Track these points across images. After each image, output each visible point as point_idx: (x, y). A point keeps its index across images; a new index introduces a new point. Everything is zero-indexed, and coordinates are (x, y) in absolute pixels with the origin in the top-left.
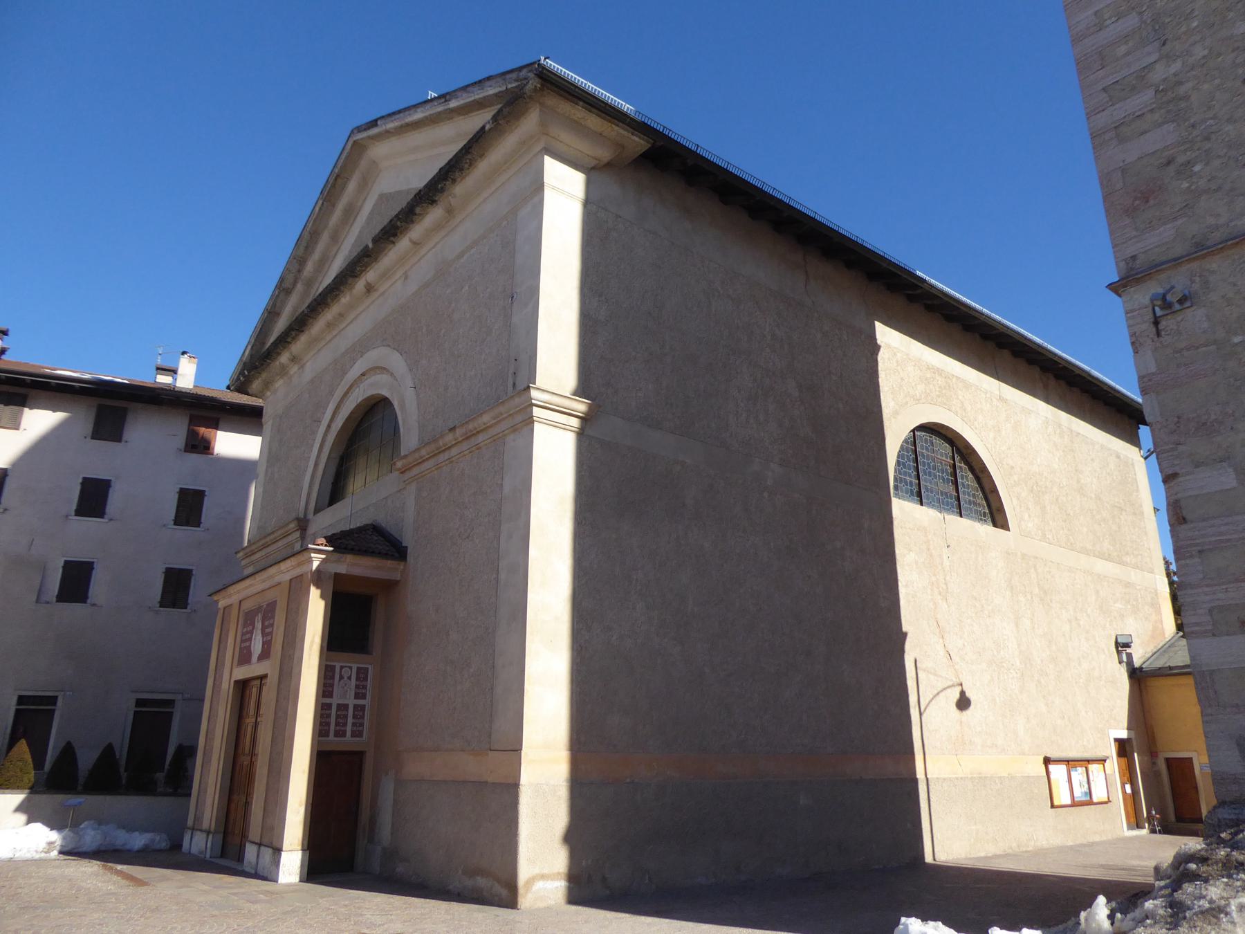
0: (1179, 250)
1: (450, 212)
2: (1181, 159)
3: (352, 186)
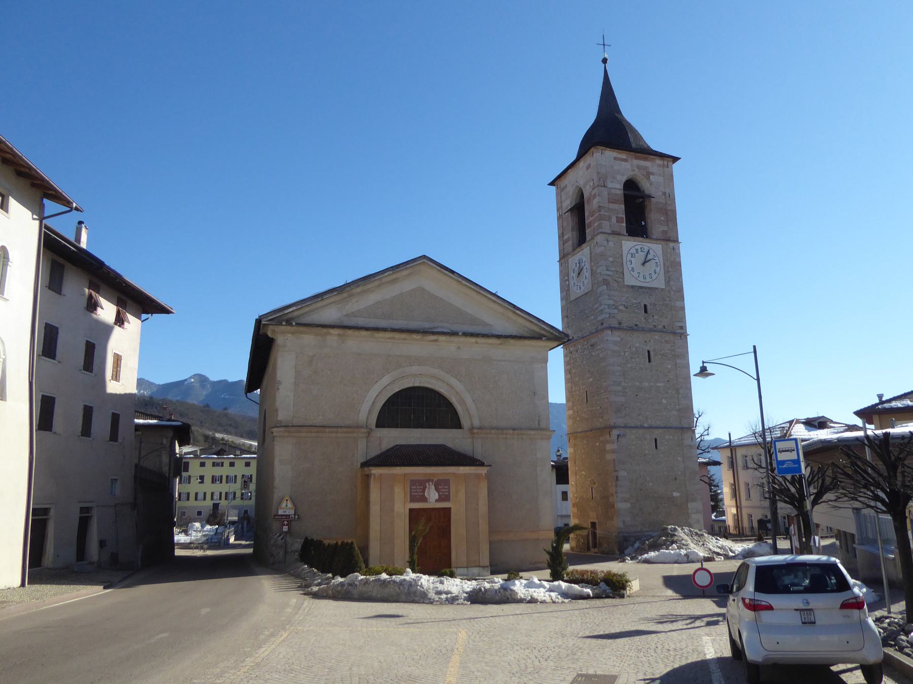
0: (623, 425)
1: (501, 344)
3: (405, 273)
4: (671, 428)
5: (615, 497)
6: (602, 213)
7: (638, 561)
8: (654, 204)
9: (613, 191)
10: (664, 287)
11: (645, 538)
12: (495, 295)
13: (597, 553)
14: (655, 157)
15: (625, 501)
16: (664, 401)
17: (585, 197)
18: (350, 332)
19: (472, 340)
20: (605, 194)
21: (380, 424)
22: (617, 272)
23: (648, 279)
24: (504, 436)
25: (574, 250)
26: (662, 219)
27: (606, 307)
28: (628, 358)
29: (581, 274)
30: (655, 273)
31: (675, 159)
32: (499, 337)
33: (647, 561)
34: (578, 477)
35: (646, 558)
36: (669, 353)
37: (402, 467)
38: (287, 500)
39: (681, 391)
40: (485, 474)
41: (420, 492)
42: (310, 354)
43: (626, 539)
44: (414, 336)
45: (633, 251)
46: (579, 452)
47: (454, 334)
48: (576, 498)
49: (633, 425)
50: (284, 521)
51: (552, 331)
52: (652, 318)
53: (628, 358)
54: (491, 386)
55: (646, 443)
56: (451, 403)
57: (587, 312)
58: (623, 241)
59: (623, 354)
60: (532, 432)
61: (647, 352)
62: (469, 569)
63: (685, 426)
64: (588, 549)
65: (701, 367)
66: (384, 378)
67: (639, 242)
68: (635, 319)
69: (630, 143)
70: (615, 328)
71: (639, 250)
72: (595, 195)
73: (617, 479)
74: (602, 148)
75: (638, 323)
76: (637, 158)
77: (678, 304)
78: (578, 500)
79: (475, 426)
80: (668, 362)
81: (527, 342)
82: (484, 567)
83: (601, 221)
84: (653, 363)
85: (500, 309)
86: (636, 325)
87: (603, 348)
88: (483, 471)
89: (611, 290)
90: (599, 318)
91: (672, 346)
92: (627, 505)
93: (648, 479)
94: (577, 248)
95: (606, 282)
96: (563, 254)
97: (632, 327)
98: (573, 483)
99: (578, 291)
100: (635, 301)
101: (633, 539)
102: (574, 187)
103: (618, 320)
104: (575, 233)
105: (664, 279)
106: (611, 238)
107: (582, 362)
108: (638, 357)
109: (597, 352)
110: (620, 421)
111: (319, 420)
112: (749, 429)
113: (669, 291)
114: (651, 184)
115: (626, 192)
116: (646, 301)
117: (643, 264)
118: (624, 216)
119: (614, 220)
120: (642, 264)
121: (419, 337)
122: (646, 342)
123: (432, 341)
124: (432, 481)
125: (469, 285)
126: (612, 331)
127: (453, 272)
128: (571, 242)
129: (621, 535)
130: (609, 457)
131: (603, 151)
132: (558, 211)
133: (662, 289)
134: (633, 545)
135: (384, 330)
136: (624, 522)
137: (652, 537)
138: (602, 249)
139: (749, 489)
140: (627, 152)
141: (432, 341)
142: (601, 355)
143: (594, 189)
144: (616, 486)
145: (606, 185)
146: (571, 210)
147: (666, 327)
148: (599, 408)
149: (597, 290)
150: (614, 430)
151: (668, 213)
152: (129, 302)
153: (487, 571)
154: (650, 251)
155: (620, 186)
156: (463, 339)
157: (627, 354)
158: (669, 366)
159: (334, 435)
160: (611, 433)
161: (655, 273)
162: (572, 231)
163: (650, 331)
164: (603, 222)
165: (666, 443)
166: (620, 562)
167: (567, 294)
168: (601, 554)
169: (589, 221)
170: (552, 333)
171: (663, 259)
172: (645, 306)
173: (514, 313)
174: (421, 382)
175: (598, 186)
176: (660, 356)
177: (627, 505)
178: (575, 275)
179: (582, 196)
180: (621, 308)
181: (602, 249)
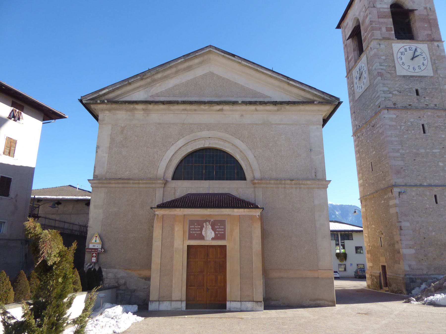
0: (403, 184)
1: (278, 110)
2: (404, 168)
3: (197, 61)
5: (400, 244)
6: (374, 25)
7: (423, 302)
8: (418, 16)
9: (381, 10)
10: (432, 75)
11: (431, 281)
13: (388, 291)
15: (410, 248)
16: (441, 164)
18: (151, 107)
19: (252, 108)
21: (175, 177)
22: (390, 66)
23: (417, 70)
24: (283, 186)
26: (426, 26)
27: (382, 92)
32: (275, 103)
33: (433, 304)
35: (431, 301)
36: (442, 126)
37: (182, 209)
38: (96, 237)
40: (259, 216)
41: (198, 231)
42: (123, 125)
43: (412, 281)
44: (203, 107)
45: (402, 50)
46: (369, 210)
47: (235, 103)
48: (370, 246)
49: (412, 184)
50: (93, 254)
52: (424, 99)
54: (271, 145)
56: (237, 160)
58: (392, 44)
59: (399, 127)
60: (309, 182)
61: (421, 125)
62: (242, 302)
64: (381, 288)
66: (179, 141)
67: (407, 43)
68: (409, 101)
70: (391, 108)
71: (408, 50)
73: (401, 229)
78: (370, 248)
79: (256, 178)
80: (442, 132)
81: (301, 107)
82: (257, 302)
83: (373, 31)
84: (428, 133)
85: (276, 83)
86: (410, 105)
88: (257, 213)
89: (385, 80)
92: (412, 251)
93: (431, 229)
95: (380, 74)
98: (366, 235)
100: (407, 87)
101: (419, 281)
103: (393, 102)
104: (356, 52)
106: (382, 42)
107: (367, 141)
108: (414, 130)
109: (377, 130)
110: (399, 181)
111: (126, 174)
113: (438, 78)
116: (418, 87)
117: (412, 59)
118: (392, 26)
119: (384, 29)
121: (206, 107)
122: (420, 117)
123: (219, 110)
124: (209, 221)
125: (247, 64)
126: (388, 110)
127: (234, 55)
129: (407, 276)
130: (393, 211)
134: (419, 287)
135: (177, 103)
136: (410, 266)
137: (438, 280)
141: (219, 110)
142: (380, 131)
144: (400, 235)
145: (375, 6)
147: (437, 105)
149: (373, 83)
150: (395, 188)
151: (431, 21)
152: (26, 106)
153: (261, 306)
156: (244, 107)
157: (403, 127)
158: (443, 136)
159: (137, 185)
160: (393, 191)
162: (354, 51)
163: (423, 109)
164: (375, 31)
166: (405, 302)
168: (391, 292)
171: (430, 55)
173: (289, 84)
174: (210, 144)
176: (434, 128)
177: (412, 251)
178: (357, 81)
179: (358, 21)
180: (395, 92)
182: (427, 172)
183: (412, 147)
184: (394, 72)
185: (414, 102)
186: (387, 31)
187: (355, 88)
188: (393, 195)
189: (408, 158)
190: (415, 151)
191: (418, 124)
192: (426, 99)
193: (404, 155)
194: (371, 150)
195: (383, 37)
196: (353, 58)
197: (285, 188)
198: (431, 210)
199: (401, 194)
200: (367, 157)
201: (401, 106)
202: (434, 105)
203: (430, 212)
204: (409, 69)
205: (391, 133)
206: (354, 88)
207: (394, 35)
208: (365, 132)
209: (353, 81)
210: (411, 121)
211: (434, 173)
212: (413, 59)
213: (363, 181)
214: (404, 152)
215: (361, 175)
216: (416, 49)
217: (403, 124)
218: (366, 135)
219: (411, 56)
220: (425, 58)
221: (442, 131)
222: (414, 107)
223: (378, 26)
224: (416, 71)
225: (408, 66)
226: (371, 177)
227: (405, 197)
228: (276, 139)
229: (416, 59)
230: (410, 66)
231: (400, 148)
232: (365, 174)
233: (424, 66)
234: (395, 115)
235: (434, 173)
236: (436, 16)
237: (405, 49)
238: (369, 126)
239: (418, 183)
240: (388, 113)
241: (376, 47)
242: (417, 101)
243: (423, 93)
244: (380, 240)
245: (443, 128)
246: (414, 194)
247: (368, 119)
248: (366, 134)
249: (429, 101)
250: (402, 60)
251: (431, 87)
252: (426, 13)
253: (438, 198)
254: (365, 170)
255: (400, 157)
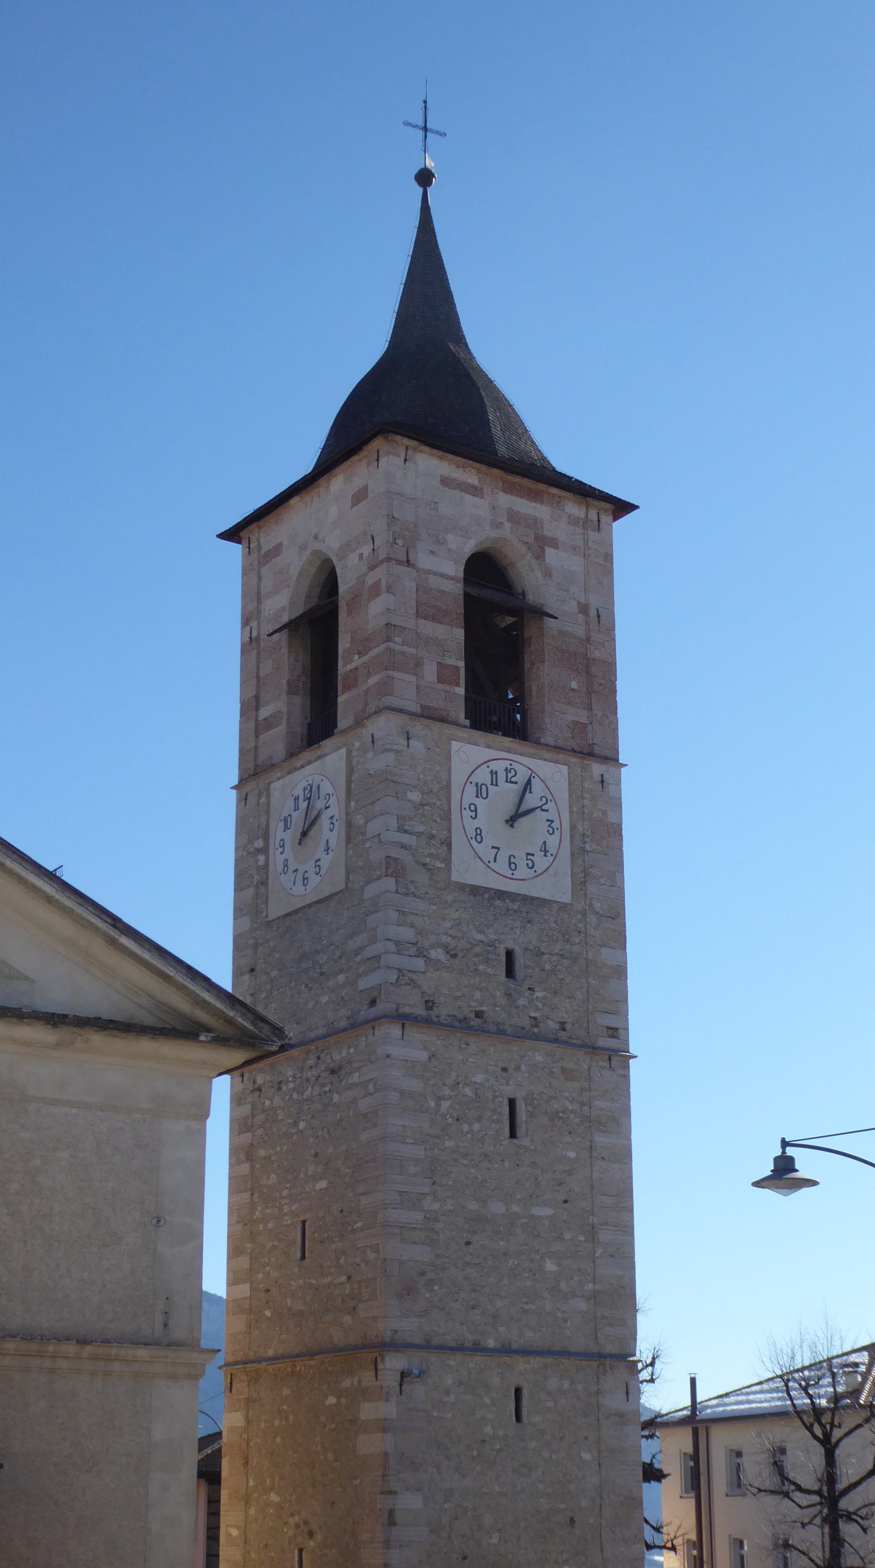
0: (418, 1339)
1: (59, 1045)
2: (430, 1275)
4: (565, 1353)
6: (397, 644)
9: (433, 582)
10: (566, 898)
12: (52, 876)
14: (563, 493)
16: (550, 1266)
17: (342, 588)
20: (410, 585)
22: (432, 837)
23: (522, 872)
24: (47, 1363)
25: (291, 754)
26: (574, 685)
27: (392, 947)
28: (450, 1121)
29: (312, 832)
30: (546, 851)
31: (622, 508)
32: (55, 1020)
34: (252, 1511)
36: (572, 1112)
39: (604, 1236)
45: (483, 776)
49: (449, 1340)
51: (231, 1014)
52: (527, 993)
53: (450, 1121)
55: (487, 1401)
57: (322, 958)
59: (432, 1104)
60: (142, 1353)
61: (506, 1102)
63: (610, 1348)
65: (777, 1160)
68: (478, 995)
69: (492, 439)
70: (415, 1020)
72: (376, 586)
73: (391, 1520)
74: (407, 442)
75: (484, 1008)
76: (510, 489)
77: (607, 955)
80: (568, 1139)
81: (146, 1045)
83: (391, 673)
84: (523, 1141)
86: (479, 1015)
87: (370, 1080)
89: (407, 895)
90: (363, 984)
91: (582, 1090)
93: (488, 1520)
94: (302, 749)
96: (251, 766)
97: (466, 1019)
98: (235, 1532)
99: (299, 889)
100: (479, 937)
102: (308, 553)
104: (297, 700)
105: (569, 872)
106: (418, 727)
107: (296, 1124)
108: (479, 1119)
112: (769, 1366)
113: (584, 914)
114: (548, 574)
115: (474, 591)
117: (512, 821)
118: (461, 664)
119: (430, 672)
120: (507, 821)
122: (505, 1070)
126: (403, 1027)
128: (282, 728)
131: (410, 452)
132: (246, 621)
133: (563, 907)
138: (389, 759)
139: (742, 1557)
140: (484, 468)
142: (364, 1105)
143: (372, 568)
144: (387, 1544)
145: (412, 562)
146: (292, 626)
147: (568, 1027)
148: (343, 1278)
149: (362, 890)
151: (594, 670)
154: (535, 782)
155: (455, 569)
157: (445, 1105)
158: (572, 1155)
160: (380, 1366)
161: (546, 851)
162: (289, 693)
163: (521, 1035)
164: (397, 674)
165: (550, 1404)
167: (257, 895)
169: (349, 667)
170: (230, 1021)
172: (510, 955)
173: (113, 942)
175: (388, 559)
176: (544, 1120)
178: (290, 836)
180: (437, 954)
181: (389, 759)
182: (503, 1294)
183: (467, 1191)
184: (443, 866)
185: (495, 1005)
186: (441, 680)
187: (271, 858)
188: (379, 1383)
189: (448, 1232)
190: (472, 1206)
191: (496, 1097)
192: (535, 996)
193: (436, 1220)
194: (311, 1169)
195: (423, 703)
196: (284, 721)
197: (52, 1371)
198: (498, 1447)
199: (409, 1378)
200: (285, 1193)
201: (449, 1016)
202: (558, 1026)
203: (494, 1453)
204: (495, 861)
205: (403, 1126)
206: (267, 859)
207: (462, 702)
208: (294, 1082)
209: (268, 825)
210: (476, 1083)
211: (525, 1300)
212: (516, 824)
213: (253, 1290)
214: (436, 1206)
215: (244, 1262)
216: (529, 782)
217: (447, 1092)
218: (295, 1096)
219: (508, 809)
220: (552, 821)
221: (570, 1133)
222: (493, 1023)
223: (413, 651)
224: (518, 874)
225: (493, 847)
226: (293, 1283)
227: (418, 1390)
228: (38, 1162)
229: (523, 822)
230: (498, 848)
231: (427, 1190)
232: (264, 1265)
233: (545, 855)
234: (426, 1053)
235: (525, 1300)
236: (613, 654)
237: (494, 773)
238: (317, 1064)
239: (469, 1338)
240: (403, 1038)
241: (395, 747)
242: (503, 1001)
243: (530, 971)
244: (297, 1558)
245: (576, 1121)
246: (450, 1382)
247: (316, 1028)
248: (294, 1089)
249: (544, 1004)
250: (476, 817)
251: (557, 948)
252: (580, 632)
253: (525, 1402)
254: (270, 1244)
255: (421, 1229)
